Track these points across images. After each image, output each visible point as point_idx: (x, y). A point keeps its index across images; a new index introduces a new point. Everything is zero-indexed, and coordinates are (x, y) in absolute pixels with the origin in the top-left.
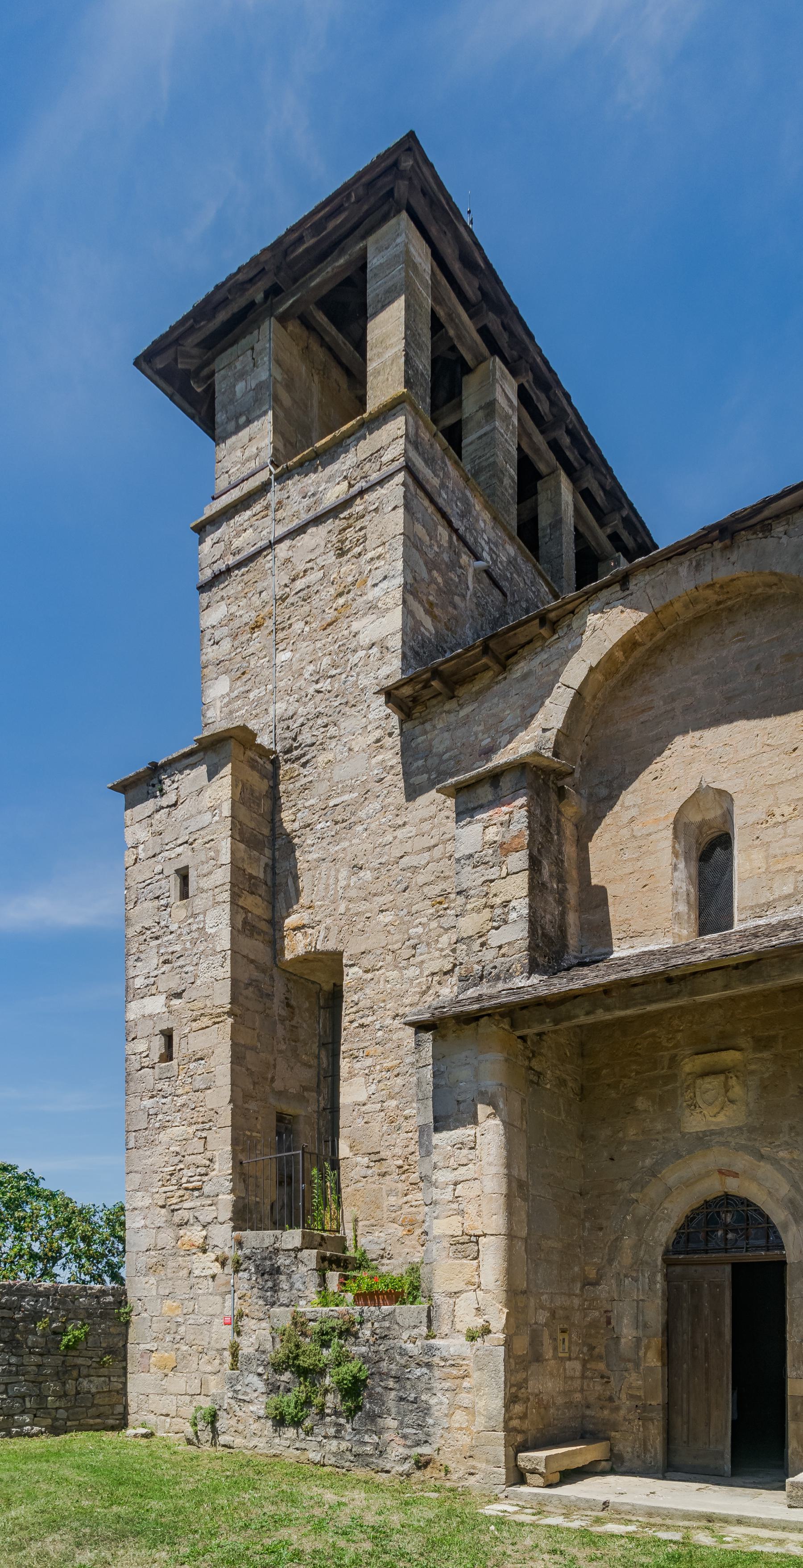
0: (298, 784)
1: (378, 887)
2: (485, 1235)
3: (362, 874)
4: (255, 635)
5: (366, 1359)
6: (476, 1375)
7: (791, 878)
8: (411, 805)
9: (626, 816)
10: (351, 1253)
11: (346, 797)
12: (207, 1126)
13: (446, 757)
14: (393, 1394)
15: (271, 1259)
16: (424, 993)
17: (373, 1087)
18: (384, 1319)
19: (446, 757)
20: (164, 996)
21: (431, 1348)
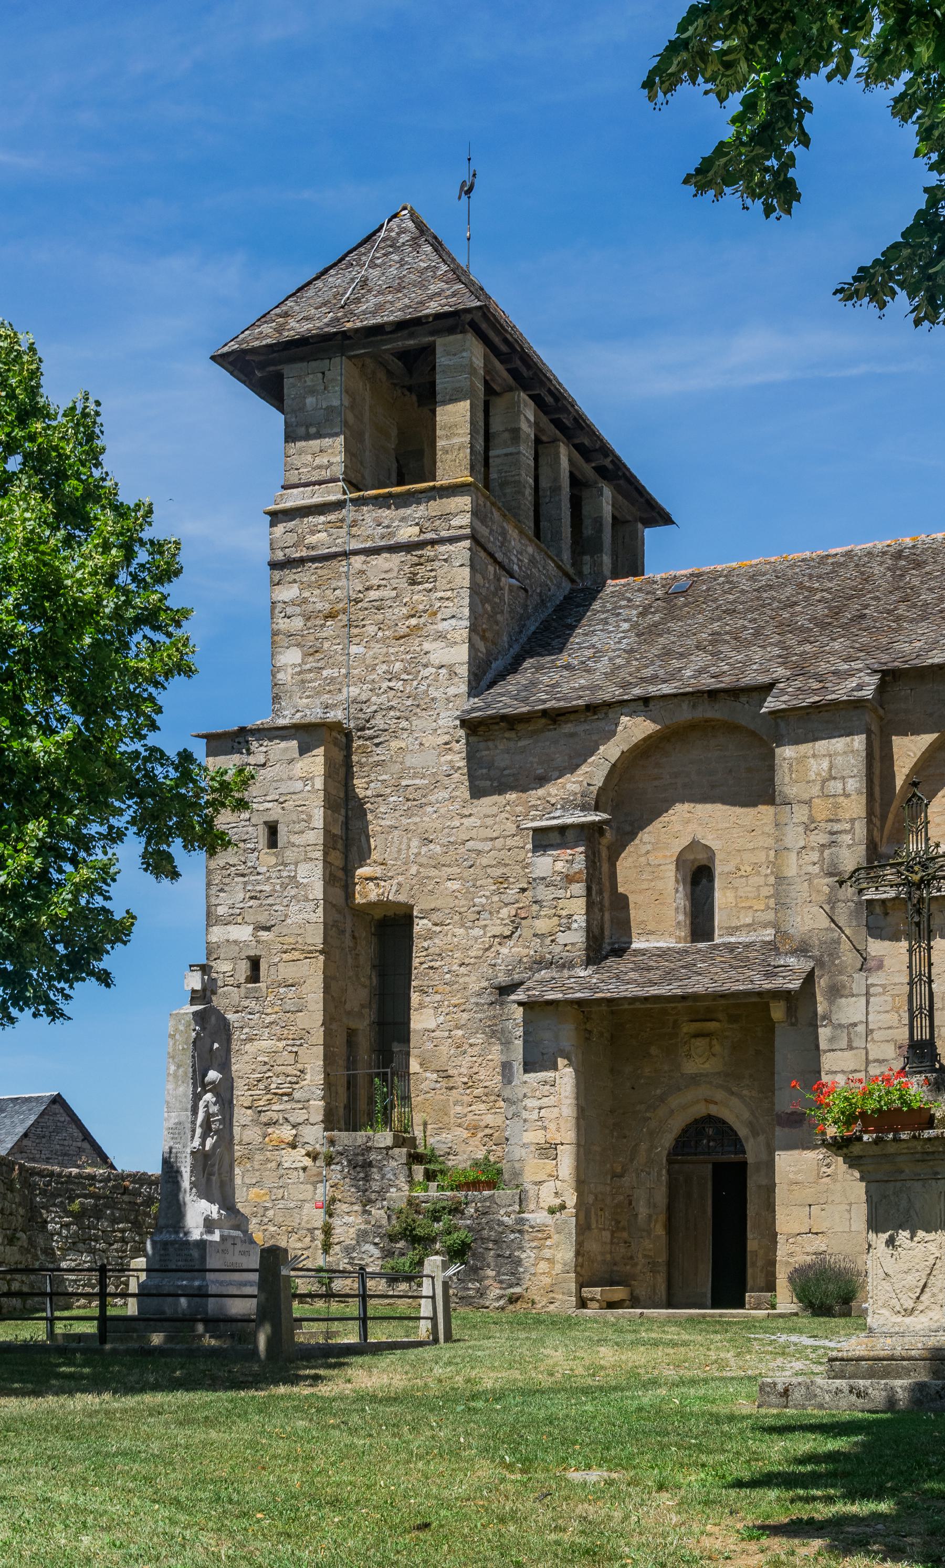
0: (371, 760)
1: (446, 860)
2: (562, 1144)
3: (432, 846)
4: (328, 623)
5: (470, 1229)
6: (556, 1237)
7: (750, 913)
8: (476, 802)
9: (644, 849)
10: (421, 1150)
11: (417, 781)
12: (298, 1042)
13: (506, 772)
14: (492, 1253)
15: (363, 1155)
16: (487, 950)
17: (442, 1018)
18: (485, 1201)
19: (506, 772)
20: (252, 927)
21: (522, 1219)
